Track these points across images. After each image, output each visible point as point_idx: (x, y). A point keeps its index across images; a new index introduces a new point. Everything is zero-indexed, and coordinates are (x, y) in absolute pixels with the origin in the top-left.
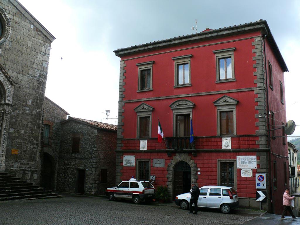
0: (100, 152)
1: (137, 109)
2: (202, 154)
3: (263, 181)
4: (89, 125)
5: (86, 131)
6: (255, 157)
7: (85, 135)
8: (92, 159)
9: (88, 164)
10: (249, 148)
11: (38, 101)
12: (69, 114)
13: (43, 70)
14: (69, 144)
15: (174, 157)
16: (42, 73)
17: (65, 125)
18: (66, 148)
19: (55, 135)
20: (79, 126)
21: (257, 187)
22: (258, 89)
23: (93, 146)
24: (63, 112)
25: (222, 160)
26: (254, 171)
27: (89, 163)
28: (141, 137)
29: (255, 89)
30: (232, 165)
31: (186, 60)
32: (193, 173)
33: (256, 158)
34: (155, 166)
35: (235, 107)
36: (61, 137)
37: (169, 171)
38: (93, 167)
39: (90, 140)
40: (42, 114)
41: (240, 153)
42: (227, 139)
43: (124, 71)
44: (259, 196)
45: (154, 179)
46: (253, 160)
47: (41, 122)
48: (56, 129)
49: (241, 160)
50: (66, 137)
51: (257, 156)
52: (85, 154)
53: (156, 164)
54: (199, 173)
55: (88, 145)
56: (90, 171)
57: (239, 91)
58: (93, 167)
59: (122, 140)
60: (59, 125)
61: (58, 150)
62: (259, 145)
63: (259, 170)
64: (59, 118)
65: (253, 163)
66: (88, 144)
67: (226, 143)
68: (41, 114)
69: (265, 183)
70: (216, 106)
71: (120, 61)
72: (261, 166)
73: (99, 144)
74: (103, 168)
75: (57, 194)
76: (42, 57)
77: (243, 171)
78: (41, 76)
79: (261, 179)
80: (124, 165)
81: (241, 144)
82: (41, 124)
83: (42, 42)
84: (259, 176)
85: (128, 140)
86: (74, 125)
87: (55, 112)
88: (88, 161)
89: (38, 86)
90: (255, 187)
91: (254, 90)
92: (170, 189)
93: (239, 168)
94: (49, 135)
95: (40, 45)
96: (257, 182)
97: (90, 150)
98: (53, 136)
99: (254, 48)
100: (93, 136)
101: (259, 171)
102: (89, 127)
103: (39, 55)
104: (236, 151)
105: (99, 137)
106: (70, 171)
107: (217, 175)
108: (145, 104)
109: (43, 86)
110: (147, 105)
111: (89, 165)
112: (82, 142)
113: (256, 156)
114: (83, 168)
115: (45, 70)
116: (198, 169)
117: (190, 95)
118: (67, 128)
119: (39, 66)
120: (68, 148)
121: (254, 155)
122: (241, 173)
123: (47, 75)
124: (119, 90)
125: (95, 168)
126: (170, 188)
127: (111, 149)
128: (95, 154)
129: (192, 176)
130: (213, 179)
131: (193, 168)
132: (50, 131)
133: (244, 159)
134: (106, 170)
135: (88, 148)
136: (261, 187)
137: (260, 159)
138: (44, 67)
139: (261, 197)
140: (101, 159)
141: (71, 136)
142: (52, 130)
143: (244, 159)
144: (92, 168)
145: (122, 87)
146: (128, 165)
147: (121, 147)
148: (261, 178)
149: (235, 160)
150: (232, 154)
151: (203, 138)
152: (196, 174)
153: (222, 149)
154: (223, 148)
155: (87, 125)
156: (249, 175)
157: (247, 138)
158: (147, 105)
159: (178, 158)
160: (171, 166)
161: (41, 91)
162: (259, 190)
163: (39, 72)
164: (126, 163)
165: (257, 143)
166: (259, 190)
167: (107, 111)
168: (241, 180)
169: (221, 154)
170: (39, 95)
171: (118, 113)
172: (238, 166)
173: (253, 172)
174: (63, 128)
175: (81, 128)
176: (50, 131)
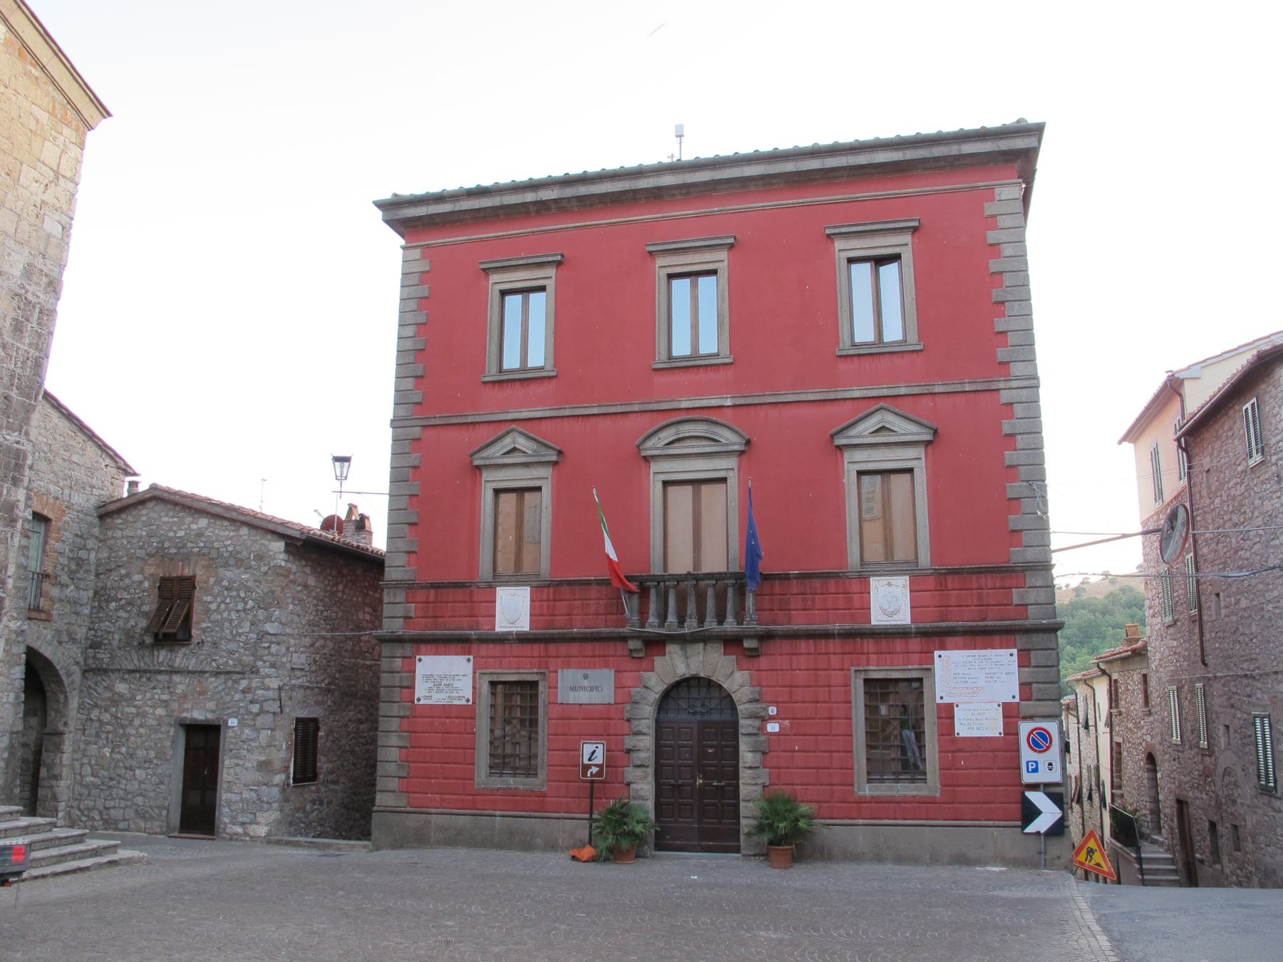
0: (292, 641)
1: (485, 453)
2: (778, 641)
4: (243, 518)
5: (230, 549)
7: (226, 565)
8: (257, 672)
9: (237, 697)
10: (984, 620)
11: (14, 394)
12: (135, 474)
13: (42, 248)
15: (658, 661)
16: (39, 263)
17: (119, 521)
18: (121, 623)
19: (68, 566)
20: (194, 527)
21: (1027, 778)
22: (1015, 384)
23: (261, 614)
24: (108, 461)
26: (1011, 714)
27: (243, 692)
29: (1002, 385)
30: (917, 685)
31: (707, 256)
32: (745, 725)
33: (1015, 657)
34: (571, 701)
35: (920, 452)
36: (97, 575)
37: (637, 722)
38: (262, 711)
39: (249, 590)
40: (30, 458)
41: (949, 640)
42: (889, 584)
43: (424, 291)
44: (1031, 813)
45: (599, 759)
47: (20, 495)
48: (77, 535)
50: (157, 574)
52: (224, 654)
53: (572, 694)
54: (773, 727)
55: (238, 611)
56: (247, 731)
57: (937, 389)
58: (262, 711)
59: (409, 587)
60: (90, 518)
61: (81, 633)
63: (1028, 707)
64: (92, 487)
66: (240, 606)
67: (890, 602)
68: (25, 458)
70: (840, 448)
71: (404, 248)
72: (1039, 690)
73: (291, 607)
74: (304, 714)
75: (116, 846)
76: (42, 188)
78: (35, 278)
80: (419, 700)
81: (953, 603)
82: (22, 505)
83: (44, 117)
84: (1031, 732)
85: (437, 586)
86: (165, 519)
87: (75, 458)
88: (236, 682)
89: (14, 319)
90: (1020, 775)
91: (998, 390)
92: (642, 798)
93: (946, 700)
94: (42, 563)
95: (33, 125)
96: (1027, 754)
97: (251, 631)
98: (59, 567)
99: (995, 227)
100: (264, 569)
102: (244, 531)
103: (27, 176)
104: (931, 635)
105: (292, 577)
106: (142, 731)
108: (521, 433)
109: (39, 324)
110: (534, 439)
111: (240, 700)
112: (209, 598)
113: (1015, 651)
114: (210, 716)
115: (52, 251)
116: (766, 709)
117: (729, 403)
118: (128, 532)
119: (24, 226)
120: (132, 622)
121: (1008, 647)
123: (61, 274)
124: (397, 371)
125: (274, 713)
126: (642, 793)
127: (333, 630)
128: (274, 649)
129: (742, 740)
131: (748, 706)
132: (46, 542)
134: (315, 720)
135: (239, 625)
136: (1043, 776)
137: (1033, 663)
138: (49, 236)
140: (298, 673)
141: (150, 570)
142: (58, 540)
144: (258, 714)
145: (411, 359)
146: (439, 698)
147: (407, 618)
150: (915, 644)
151: (786, 577)
152: (762, 729)
153: (874, 622)
154: (878, 618)
155: (232, 521)
157: (974, 577)
158: (534, 439)
159: (676, 664)
160: (644, 699)
161: (30, 345)
162: (1034, 787)
163: (26, 253)
164: (430, 689)
165: (1016, 600)
166: (1034, 787)
167: (337, 459)
168: (959, 751)
169: (869, 645)
170: (19, 364)
171: (389, 469)
174: (110, 533)
175: (200, 534)
176: (46, 542)
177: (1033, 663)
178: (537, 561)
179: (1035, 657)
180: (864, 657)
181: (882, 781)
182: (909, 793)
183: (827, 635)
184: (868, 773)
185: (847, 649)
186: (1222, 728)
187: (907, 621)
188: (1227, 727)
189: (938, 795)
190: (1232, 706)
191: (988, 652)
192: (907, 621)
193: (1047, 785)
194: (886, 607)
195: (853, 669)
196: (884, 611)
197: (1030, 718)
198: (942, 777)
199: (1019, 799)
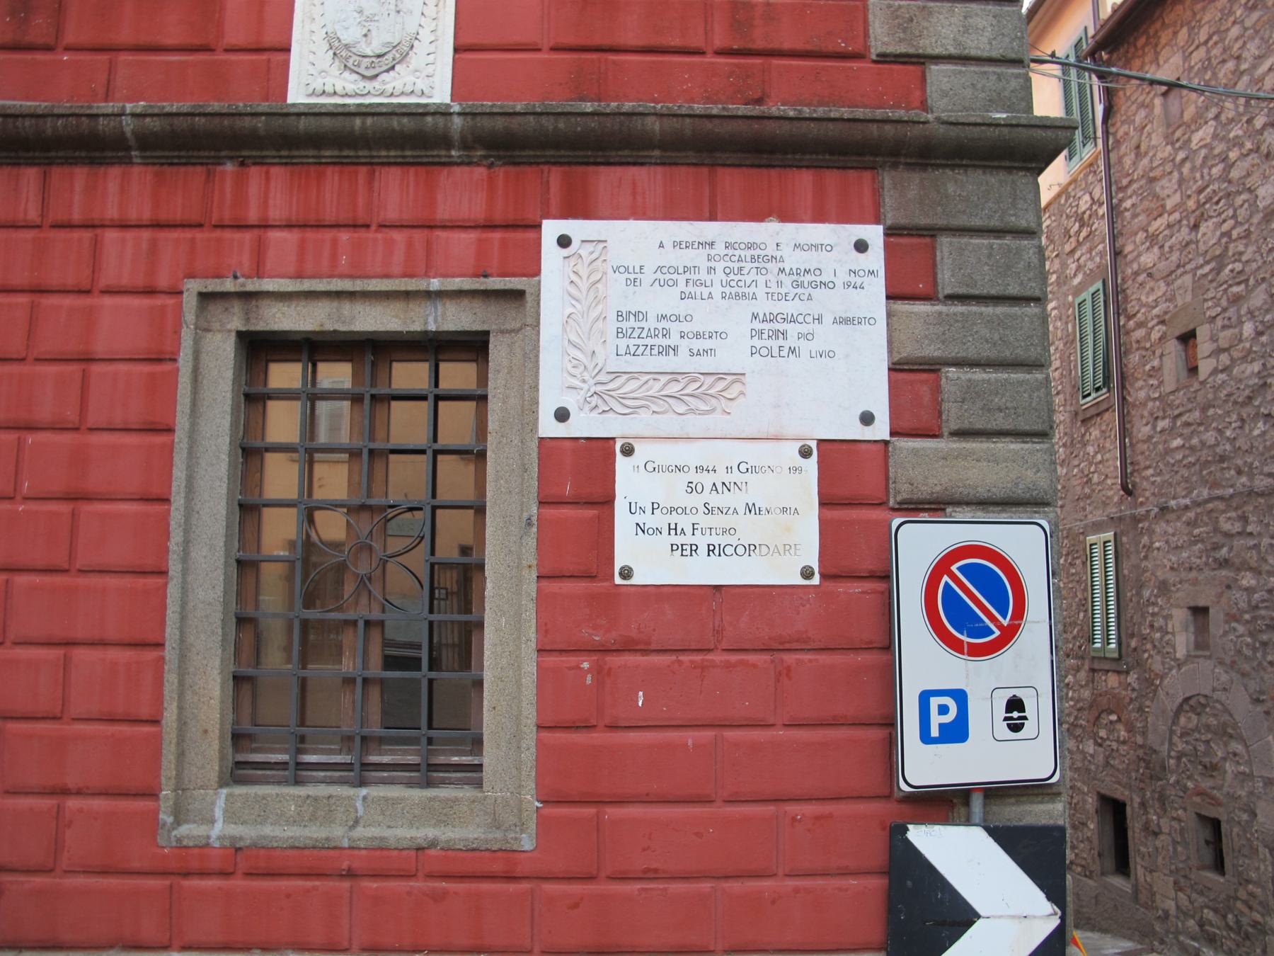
3: (1006, 658)
6: (861, 246)
14: (1119, 720)
21: (925, 766)
25: (269, 285)
26: (853, 487)
28: (246, 462)
33: (876, 258)
41: (606, 180)
46: (831, 302)
49: (617, 283)
51: (890, 233)
62: (920, 60)
63: (923, 462)
65: (827, 336)
69: (1042, 677)
72: (970, 393)
77: (670, 490)
79: (976, 606)
93: (583, 426)
96: (924, 661)
101: (933, 482)
107: (174, 568)
113: (874, 234)
121: (845, 217)
122: (623, 523)
130: (80, 633)
133: (666, 277)
136: (989, 757)
139: (979, 924)
143: (666, 277)
148: (975, 599)
149: (518, 295)
150: (463, 191)
156: (750, 549)
162: (945, 804)
166: (945, 804)
168: (628, 647)
169: (271, 191)
172: (570, 402)
173: (826, 502)
177: (948, 280)
178: (444, 753)
179: (954, 263)
180: (248, 236)
181: (297, 773)
182: (403, 833)
183: (91, 146)
184: (239, 738)
185: (176, 209)
186: (1180, 615)
187: (439, 92)
188: (1199, 612)
189: (527, 843)
190: (1224, 564)
191: (769, 232)
192: (439, 92)
193: (996, 793)
194: (350, 34)
195: (193, 287)
196: (341, 52)
197: (932, 507)
198: (550, 765)
199: (876, 853)
